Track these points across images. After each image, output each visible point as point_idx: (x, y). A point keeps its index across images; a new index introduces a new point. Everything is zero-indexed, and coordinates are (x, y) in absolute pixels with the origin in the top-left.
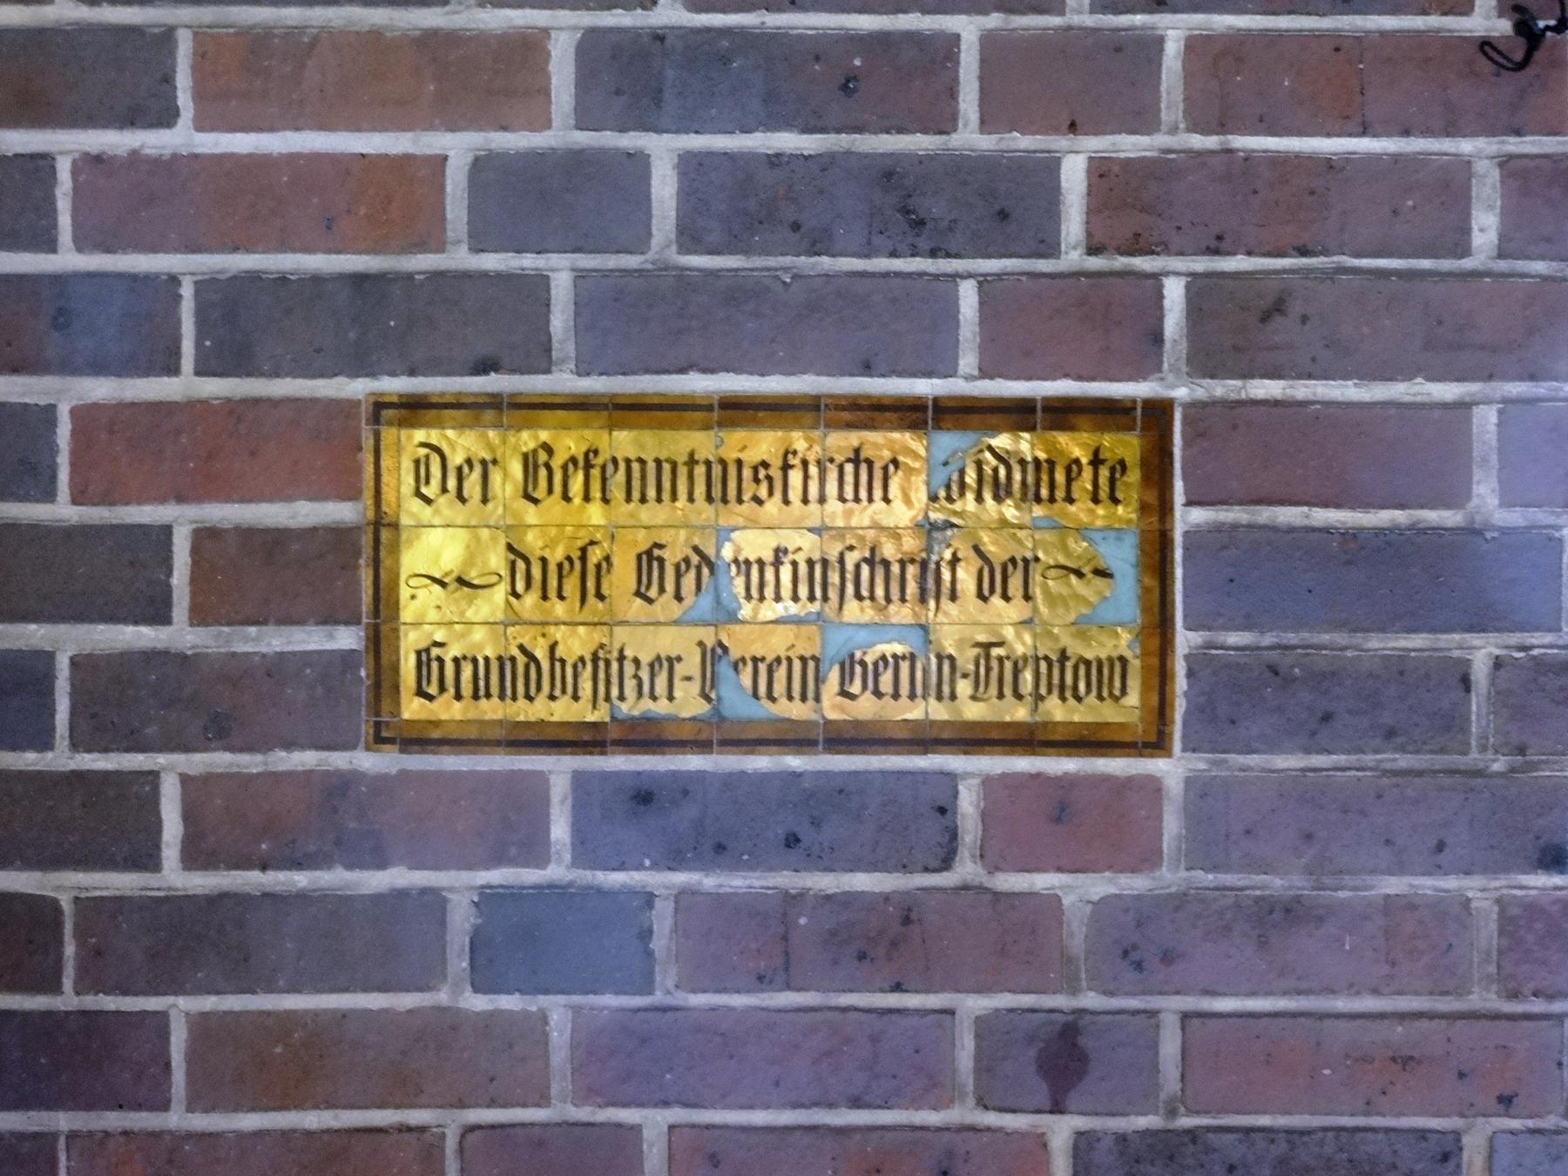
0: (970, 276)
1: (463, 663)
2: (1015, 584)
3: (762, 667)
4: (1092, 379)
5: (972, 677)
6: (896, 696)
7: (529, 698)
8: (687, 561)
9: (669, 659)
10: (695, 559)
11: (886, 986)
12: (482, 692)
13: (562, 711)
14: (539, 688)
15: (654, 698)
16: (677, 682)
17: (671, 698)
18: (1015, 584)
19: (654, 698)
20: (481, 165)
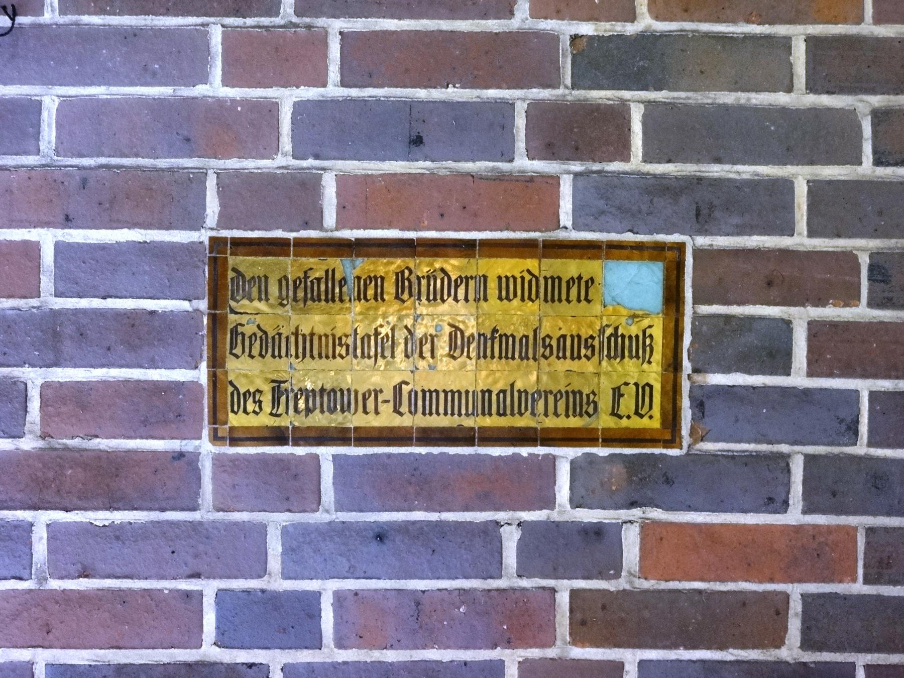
0: (569, 173)
1: (549, 395)
2: (427, 348)
3: (551, 399)
4: (444, 230)
5: (392, 403)
6: (546, 415)
7: (521, 414)
8: (255, 334)
9: (375, 391)
10: (259, 334)
11: (73, 569)
12: (427, 412)
13: (373, 421)
14: (526, 409)
15: (556, 414)
16: (379, 404)
17: (377, 412)
18: (427, 348)
19: (556, 414)
20: (300, 108)
